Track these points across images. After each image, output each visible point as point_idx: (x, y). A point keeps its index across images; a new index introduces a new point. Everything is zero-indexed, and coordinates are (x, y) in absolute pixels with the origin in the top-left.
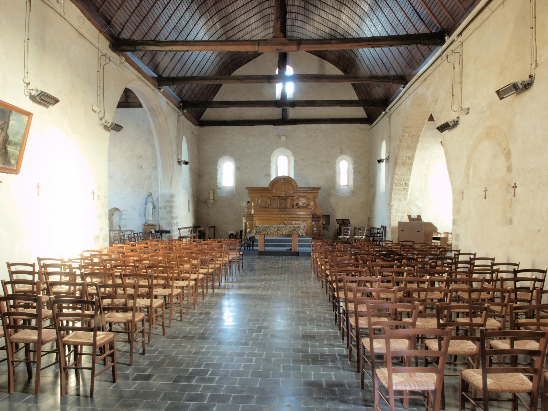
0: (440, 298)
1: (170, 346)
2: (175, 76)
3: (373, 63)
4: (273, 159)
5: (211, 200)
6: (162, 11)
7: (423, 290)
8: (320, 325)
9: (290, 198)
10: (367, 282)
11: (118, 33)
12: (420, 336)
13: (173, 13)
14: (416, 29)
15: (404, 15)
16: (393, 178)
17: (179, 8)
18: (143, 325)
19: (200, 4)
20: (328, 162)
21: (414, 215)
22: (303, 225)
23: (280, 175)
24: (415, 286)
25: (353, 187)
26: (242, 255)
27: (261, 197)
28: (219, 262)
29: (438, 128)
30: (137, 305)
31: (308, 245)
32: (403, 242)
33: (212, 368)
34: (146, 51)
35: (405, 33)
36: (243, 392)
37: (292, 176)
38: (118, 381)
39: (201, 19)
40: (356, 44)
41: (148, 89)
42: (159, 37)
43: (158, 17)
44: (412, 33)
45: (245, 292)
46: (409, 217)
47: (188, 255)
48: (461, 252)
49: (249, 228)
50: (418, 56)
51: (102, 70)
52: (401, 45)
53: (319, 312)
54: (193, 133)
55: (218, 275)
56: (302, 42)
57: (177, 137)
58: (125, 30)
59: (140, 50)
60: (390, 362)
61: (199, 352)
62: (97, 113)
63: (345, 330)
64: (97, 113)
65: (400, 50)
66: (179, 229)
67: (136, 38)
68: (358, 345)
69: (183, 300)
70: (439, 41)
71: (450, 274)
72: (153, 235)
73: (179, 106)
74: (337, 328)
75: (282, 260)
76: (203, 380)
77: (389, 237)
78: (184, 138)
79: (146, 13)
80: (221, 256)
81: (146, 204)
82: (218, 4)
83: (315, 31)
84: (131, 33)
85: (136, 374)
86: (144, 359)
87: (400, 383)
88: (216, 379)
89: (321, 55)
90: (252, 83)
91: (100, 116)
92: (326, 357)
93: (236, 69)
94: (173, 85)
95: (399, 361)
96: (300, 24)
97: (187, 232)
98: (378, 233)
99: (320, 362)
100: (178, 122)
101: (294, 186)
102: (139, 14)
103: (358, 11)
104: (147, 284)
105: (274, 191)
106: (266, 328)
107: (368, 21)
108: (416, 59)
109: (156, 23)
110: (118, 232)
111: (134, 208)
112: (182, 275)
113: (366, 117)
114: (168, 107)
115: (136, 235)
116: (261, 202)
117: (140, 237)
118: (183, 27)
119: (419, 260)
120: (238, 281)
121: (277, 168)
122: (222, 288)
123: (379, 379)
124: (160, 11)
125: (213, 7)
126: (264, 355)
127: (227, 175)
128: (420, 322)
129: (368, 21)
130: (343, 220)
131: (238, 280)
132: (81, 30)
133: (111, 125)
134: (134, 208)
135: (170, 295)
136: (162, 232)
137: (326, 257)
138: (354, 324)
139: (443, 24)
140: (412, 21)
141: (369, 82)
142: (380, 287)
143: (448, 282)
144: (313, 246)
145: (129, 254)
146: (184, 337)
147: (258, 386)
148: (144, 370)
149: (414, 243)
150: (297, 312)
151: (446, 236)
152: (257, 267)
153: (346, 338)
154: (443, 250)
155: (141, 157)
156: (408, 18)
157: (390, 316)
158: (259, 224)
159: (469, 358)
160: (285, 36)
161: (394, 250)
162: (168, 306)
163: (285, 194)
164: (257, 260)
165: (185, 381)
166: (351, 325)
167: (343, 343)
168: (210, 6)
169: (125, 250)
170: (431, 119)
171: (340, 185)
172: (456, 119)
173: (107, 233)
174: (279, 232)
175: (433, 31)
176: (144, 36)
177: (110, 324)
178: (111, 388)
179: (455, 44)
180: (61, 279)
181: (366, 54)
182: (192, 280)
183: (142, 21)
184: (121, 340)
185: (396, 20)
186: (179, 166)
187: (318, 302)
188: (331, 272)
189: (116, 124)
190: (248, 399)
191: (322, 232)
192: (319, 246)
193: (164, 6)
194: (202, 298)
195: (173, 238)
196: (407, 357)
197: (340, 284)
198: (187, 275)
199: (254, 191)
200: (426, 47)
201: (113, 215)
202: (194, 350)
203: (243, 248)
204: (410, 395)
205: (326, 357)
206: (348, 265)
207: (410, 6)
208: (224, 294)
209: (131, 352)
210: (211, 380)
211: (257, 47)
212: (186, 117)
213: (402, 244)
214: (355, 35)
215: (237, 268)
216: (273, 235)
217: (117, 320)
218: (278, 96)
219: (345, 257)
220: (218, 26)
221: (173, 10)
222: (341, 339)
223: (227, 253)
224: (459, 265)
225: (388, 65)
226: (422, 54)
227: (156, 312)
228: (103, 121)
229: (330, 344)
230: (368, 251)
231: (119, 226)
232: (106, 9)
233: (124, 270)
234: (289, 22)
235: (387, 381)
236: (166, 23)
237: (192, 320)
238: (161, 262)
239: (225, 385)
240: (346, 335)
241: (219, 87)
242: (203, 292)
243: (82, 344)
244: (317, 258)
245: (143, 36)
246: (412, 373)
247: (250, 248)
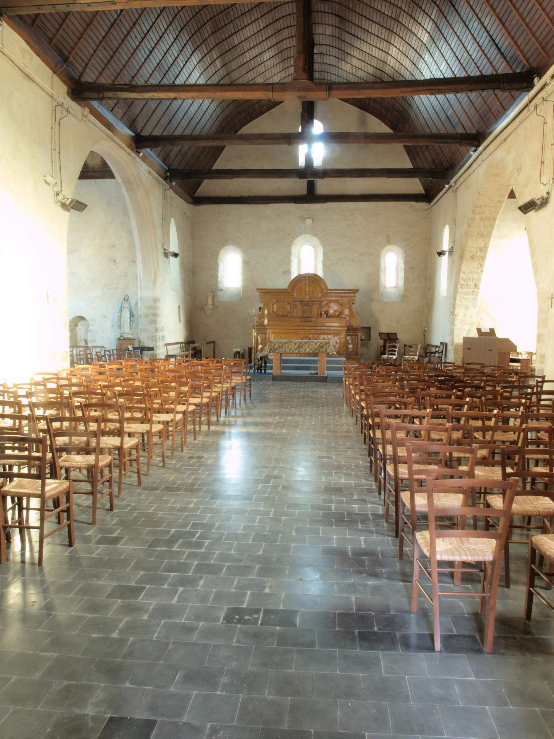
0: (512, 440)
1: (148, 499)
2: (159, 134)
3: (434, 116)
4: (294, 250)
5: (210, 306)
6: (140, 43)
7: (489, 428)
8: (350, 475)
9: (316, 304)
10: (417, 417)
11: (79, 74)
12: (483, 490)
13: (156, 45)
14: (494, 67)
15: (478, 48)
16: (458, 277)
17: (163, 39)
18: (110, 472)
19: (193, 32)
20: (370, 255)
21: (485, 329)
22: (334, 341)
23: (303, 272)
24: (479, 423)
25: (403, 289)
26: (250, 380)
27: (277, 301)
28: (217, 389)
29: (520, 208)
30: (102, 445)
31: (339, 368)
32: (468, 364)
33: (201, 529)
34: (118, 99)
35: (478, 74)
36: (241, 561)
37: (320, 273)
38: (76, 545)
39: (195, 54)
40: (409, 89)
41: (122, 153)
42: (136, 79)
43: (135, 51)
44: (488, 73)
45: (251, 429)
46: (479, 330)
47: (174, 379)
48: (546, 379)
49: (261, 344)
50: (496, 106)
51: (57, 126)
52: (471, 91)
53: (349, 457)
54: (185, 213)
55: (216, 407)
56: (334, 86)
57: (163, 219)
58: (88, 70)
59: (110, 98)
60: (432, 523)
61: (186, 508)
62: (51, 186)
63: (382, 481)
64: (51, 186)
65: (471, 98)
66: (166, 345)
67: (104, 82)
68: (397, 501)
69: (168, 439)
70: (525, 85)
71: (527, 408)
72: (130, 353)
73: (165, 176)
74: (372, 478)
75: (304, 387)
76: (189, 545)
77: (451, 357)
78: (173, 221)
79: (117, 45)
80: (220, 382)
81: (121, 311)
82: (218, 33)
83: (354, 70)
84: (97, 74)
85: (100, 536)
86: (112, 516)
87: (447, 551)
88: (206, 544)
89: (364, 105)
90: (266, 144)
91: (55, 189)
92: (355, 516)
93: (245, 125)
94: (156, 147)
95: (447, 523)
96: (333, 61)
97: (177, 349)
98: (435, 352)
99: (346, 524)
100: (164, 198)
101: (323, 287)
102: (107, 47)
103: (414, 42)
104: (117, 417)
105: (295, 294)
106: (277, 477)
107: (427, 57)
108: (493, 110)
109: (132, 59)
110: (83, 349)
111: (105, 317)
112: (166, 406)
113: (423, 192)
114: (150, 177)
115: (107, 353)
116: (278, 309)
117: (113, 355)
118: (169, 65)
119: (488, 388)
120: (243, 416)
121: (299, 262)
122: (220, 425)
123: (419, 546)
124: (137, 43)
125: (212, 37)
126: (272, 514)
127: (231, 272)
128: (480, 472)
129: (427, 57)
130: (388, 334)
131: (243, 414)
132: (27, 70)
133: (72, 202)
134: (105, 317)
135: (148, 432)
136: (142, 349)
137: (362, 384)
138: (392, 473)
139: (531, 60)
140: (489, 56)
141: (427, 144)
142: (431, 424)
143: (524, 419)
144: (345, 369)
145: (96, 378)
146: (167, 489)
147: (261, 553)
148: (112, 531)
149: (483, 366)
150: (319, 457)
151: (529, 358)
152: (271, 396)
153: (383, 492)
154: (523, 375)
155: (114, 246)
156: (483, 51)
157: (440, 463)
159: (545, 520)
160: (311, 77)
161: (455, 375)
162: (146, 446)
163: (310, 298)
164: (271, 387)
165: (164, 546)
166: (389, 475)
167: (380, 498)
168: (207, 36)
169: (90, 372)
170: (512, 195)
171: (385, 287)
172: (545, 195)
173: (68, 349)
174: (301, 349)
175: (518, 71)
176: (116, 78)
177: (67, 470)
178: (66, 553)
179: (548, 89)
180: (3, 411)
181: (426, 104)
182: (180, 412)
183: (112, 57)
184: (82, 491)
185: (466, 54)
186: (166, 259)
187: (348, 444)
188: (367, 404)
189: (78, 202)
190: (247, 569)
191: (360, 350)
192: (353, 369)
193: (143, 36)
194: (193, 438)
195: (158, 357)
196: (461, 516)
197: (377, 420)
198: (173, 406)
199: (267, 294)
200: (507, 93)
201: (76, 325)
202: (178, 506)
203: (252, 371)
204: (463, 568)
205: (355, 516)
206: (390, 394)
207: (486, 34)
208: (223, 433)
209: (94, 507)
210: (199, 545)
211: (270, 93)
212: (174, 191)
213: (466, 368)
214: (408, 77)
215: (242, 398)
216: (293, 353)
217: (74, 464)
218: (302, 163)
219: (386, 384)
220: (218, 64)
221: (156, 41)
222: (377, 494)
223: (229, 377)
224: (544, 397)
225: (455, 120)
226: (501, 103)
227: (130, 454)
228: (60, 197)
229: (362, 500)
230: (419, 376)
231: (86, 341)
232: (61, 40)
233: (87, 398)
234: (317, 59)
235: (429, 548)
236: (146, 60)
237: (177, 466)
238: (138, 388)
239: (217, 552)
240: (383, 488)
241: (220, 149)
242: (194, 429)
243: (29, 496)
244: (350, 384)
245: (113, 78)
246: (464, 539)
247: (261, 370)
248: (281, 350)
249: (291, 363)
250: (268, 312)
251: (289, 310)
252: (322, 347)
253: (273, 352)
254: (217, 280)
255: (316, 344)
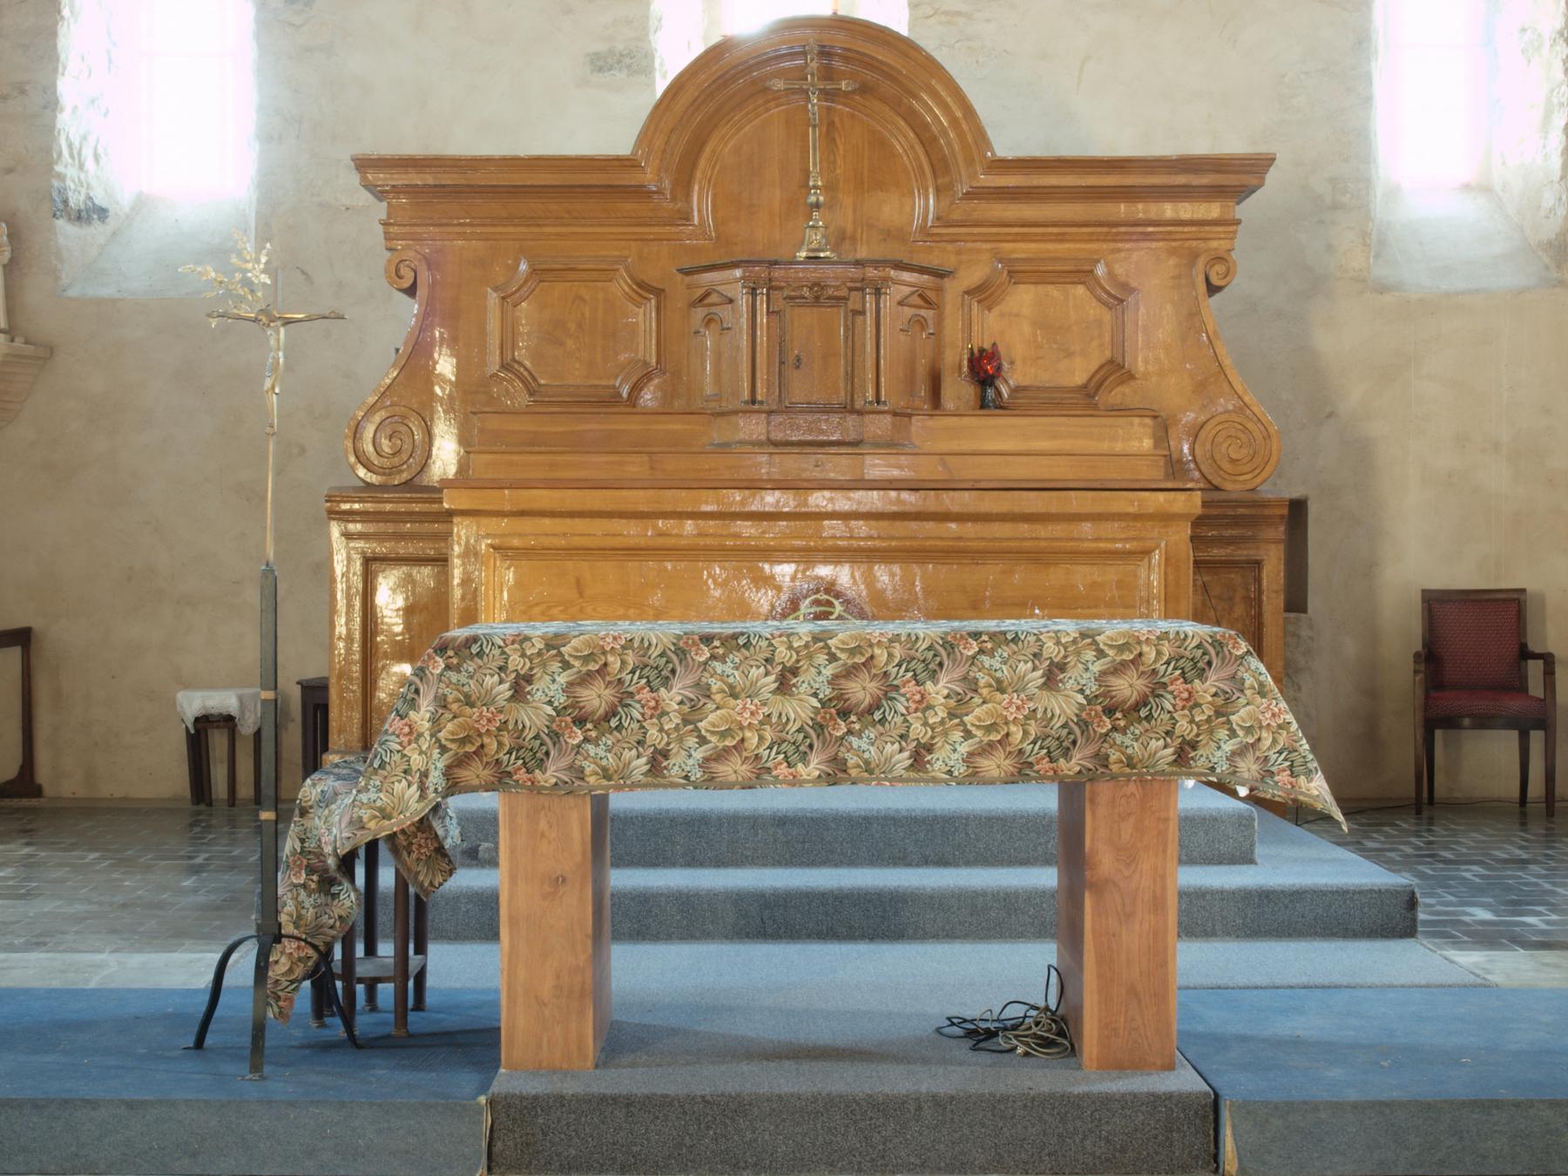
158: (523, 609)
199: (453, 207)
248: (600, 754)
249: (693, 861)
250: (460, 369)
251: (648, 351)
252: (1137, 710)
253: (500, 779)
254: (50, 130)
255: (1053, 676)
